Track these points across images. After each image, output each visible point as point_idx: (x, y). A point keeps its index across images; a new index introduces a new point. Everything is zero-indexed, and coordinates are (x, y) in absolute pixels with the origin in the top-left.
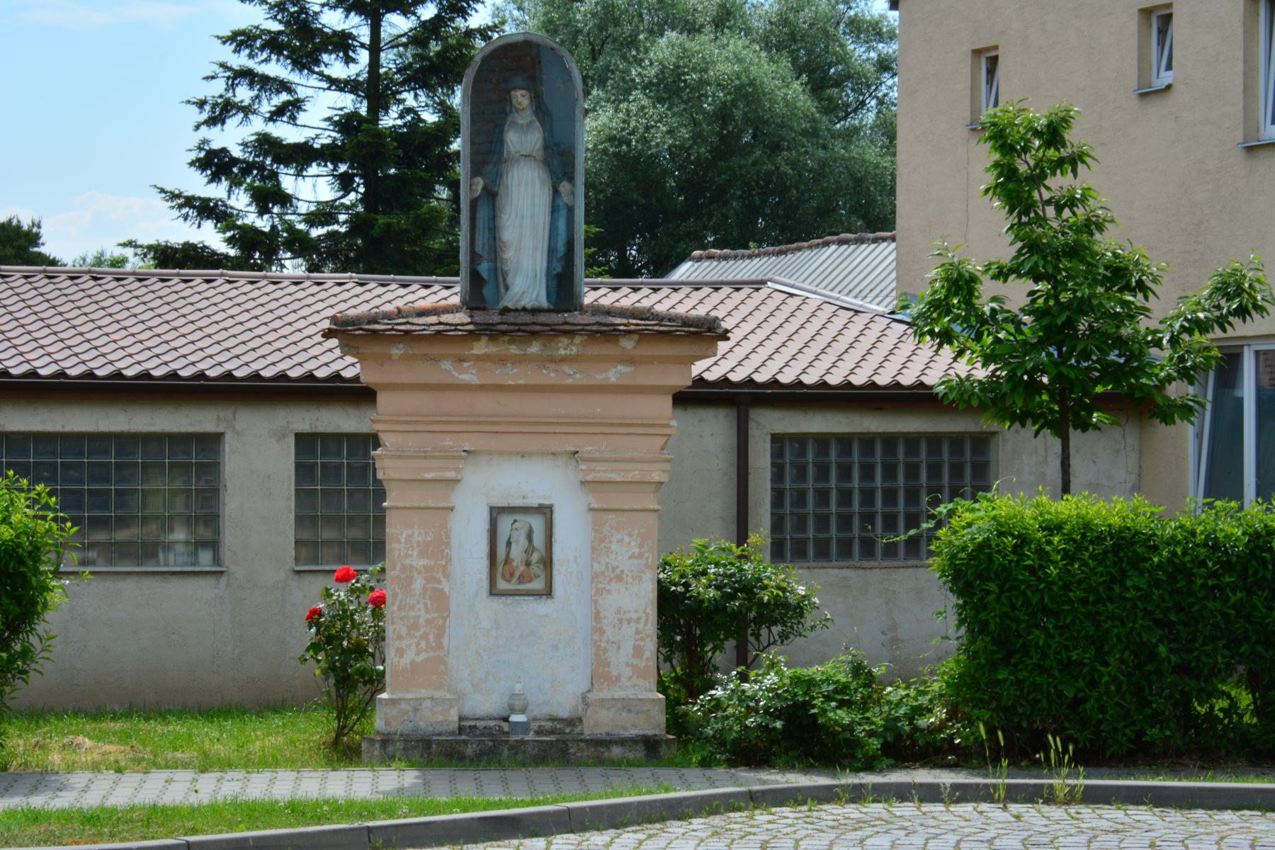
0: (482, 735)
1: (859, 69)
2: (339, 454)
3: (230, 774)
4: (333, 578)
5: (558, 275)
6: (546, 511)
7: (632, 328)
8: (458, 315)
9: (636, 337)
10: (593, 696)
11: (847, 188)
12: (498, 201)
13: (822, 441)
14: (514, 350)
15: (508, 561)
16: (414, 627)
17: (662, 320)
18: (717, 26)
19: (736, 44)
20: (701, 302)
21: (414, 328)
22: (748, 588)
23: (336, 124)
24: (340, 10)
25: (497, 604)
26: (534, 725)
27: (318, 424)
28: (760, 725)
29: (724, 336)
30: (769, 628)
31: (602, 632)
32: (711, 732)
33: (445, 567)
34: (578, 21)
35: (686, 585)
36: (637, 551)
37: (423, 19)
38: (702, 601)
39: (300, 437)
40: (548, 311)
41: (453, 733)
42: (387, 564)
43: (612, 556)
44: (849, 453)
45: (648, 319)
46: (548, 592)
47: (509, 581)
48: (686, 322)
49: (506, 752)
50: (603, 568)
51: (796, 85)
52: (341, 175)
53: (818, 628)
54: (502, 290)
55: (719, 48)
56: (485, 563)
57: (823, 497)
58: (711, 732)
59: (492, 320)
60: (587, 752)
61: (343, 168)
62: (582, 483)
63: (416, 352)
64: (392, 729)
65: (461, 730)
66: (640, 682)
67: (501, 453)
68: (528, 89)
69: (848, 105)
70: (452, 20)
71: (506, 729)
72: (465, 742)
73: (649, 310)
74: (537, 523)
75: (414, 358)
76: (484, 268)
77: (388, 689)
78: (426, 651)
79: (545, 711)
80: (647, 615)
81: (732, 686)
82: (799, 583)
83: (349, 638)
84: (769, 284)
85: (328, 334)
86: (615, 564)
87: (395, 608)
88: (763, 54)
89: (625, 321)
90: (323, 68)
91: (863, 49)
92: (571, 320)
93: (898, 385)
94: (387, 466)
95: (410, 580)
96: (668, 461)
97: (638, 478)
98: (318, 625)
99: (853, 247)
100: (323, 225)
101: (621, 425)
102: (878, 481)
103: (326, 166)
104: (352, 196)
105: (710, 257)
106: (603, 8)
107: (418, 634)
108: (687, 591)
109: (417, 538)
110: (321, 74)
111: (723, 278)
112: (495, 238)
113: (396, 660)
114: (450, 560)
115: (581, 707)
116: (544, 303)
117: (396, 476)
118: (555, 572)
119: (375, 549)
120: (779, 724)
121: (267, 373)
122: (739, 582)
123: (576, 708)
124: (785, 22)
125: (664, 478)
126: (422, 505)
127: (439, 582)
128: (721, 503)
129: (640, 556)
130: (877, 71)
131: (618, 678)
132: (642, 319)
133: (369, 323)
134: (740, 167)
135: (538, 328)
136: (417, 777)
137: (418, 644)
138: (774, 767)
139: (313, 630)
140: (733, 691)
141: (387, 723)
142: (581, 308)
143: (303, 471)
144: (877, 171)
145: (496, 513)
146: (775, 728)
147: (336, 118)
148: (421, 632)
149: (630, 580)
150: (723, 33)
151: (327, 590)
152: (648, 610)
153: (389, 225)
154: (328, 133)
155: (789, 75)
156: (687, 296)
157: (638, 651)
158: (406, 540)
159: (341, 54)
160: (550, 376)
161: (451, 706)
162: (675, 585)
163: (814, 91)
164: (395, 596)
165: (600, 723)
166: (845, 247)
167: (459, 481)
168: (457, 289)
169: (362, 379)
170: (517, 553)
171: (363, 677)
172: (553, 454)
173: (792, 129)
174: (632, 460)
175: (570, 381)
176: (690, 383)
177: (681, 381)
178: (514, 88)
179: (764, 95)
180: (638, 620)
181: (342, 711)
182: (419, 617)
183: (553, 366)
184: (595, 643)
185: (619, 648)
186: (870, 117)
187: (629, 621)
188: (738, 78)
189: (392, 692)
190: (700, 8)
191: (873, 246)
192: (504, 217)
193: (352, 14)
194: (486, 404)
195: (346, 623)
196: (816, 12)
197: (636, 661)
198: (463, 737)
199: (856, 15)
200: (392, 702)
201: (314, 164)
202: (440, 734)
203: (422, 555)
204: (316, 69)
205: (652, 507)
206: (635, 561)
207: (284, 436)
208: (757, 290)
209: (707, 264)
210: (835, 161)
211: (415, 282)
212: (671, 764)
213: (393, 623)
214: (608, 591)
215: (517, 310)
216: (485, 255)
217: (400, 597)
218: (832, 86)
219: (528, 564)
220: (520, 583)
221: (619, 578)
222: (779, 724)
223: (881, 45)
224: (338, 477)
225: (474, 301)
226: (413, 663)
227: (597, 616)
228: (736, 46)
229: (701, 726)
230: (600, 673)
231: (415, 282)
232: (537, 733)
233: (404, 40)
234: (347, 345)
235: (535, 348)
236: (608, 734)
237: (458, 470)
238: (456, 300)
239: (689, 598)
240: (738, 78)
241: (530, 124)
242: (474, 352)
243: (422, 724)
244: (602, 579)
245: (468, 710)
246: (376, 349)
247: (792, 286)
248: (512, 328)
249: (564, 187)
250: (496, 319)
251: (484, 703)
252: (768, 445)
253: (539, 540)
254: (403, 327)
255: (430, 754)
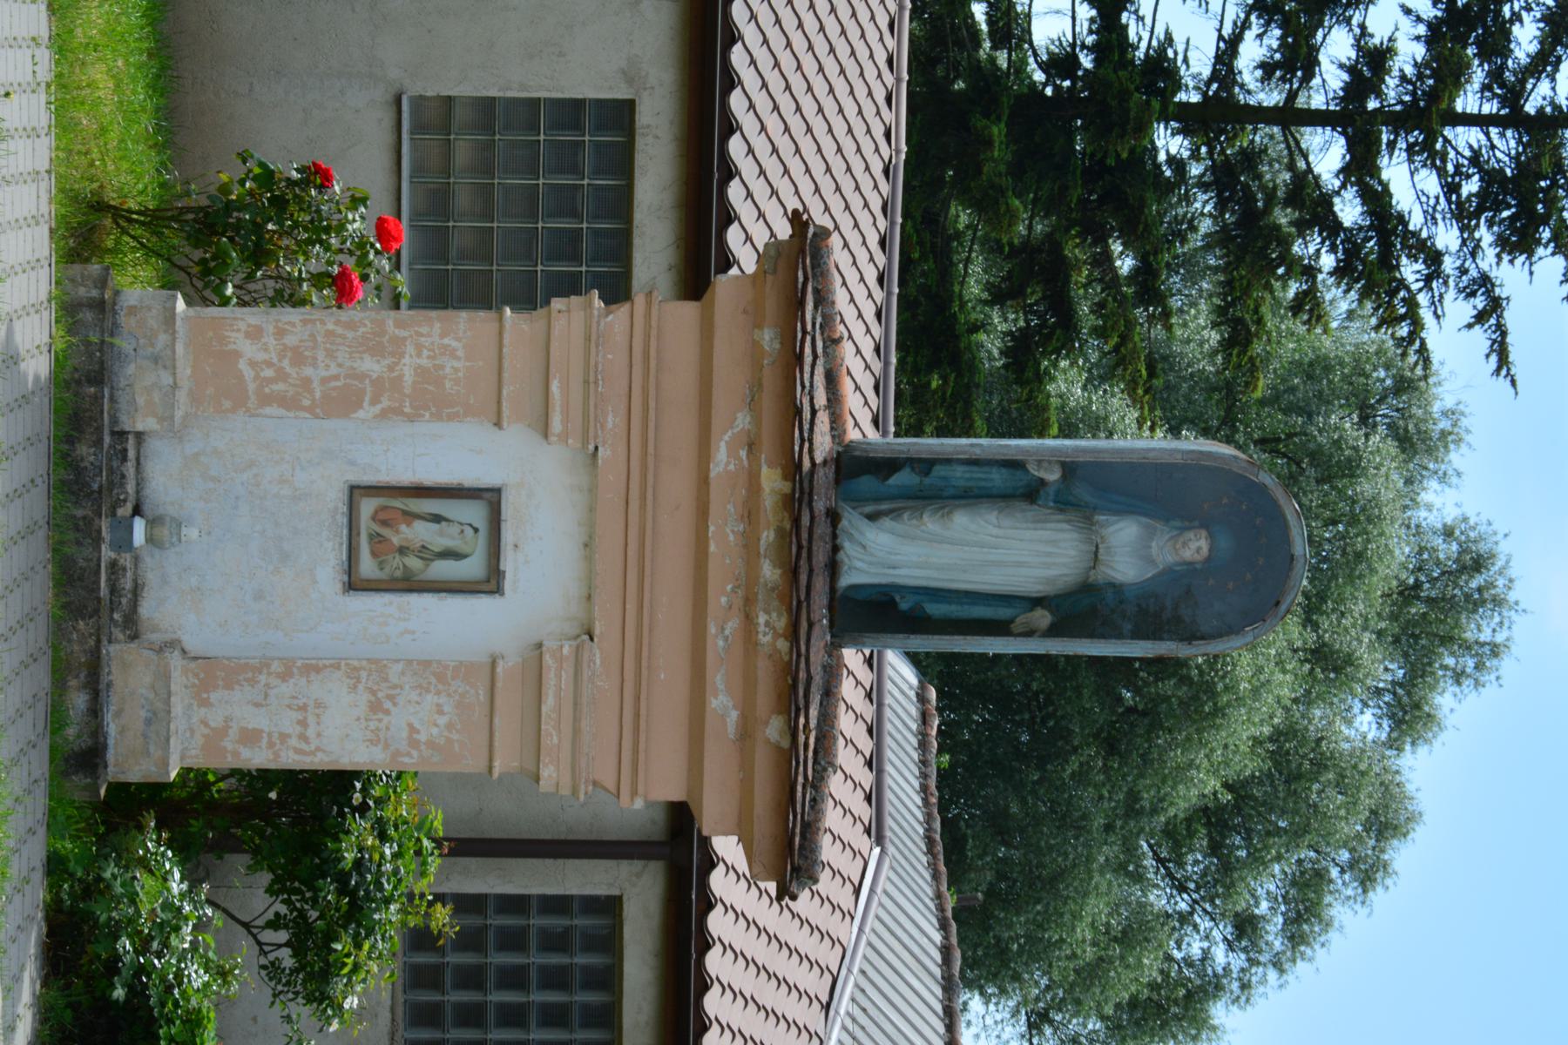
0: (111, 471)
1: (1241, 887)
2: (597, 172)
3: (44, 55)
4: (388, 214)
5: (892, 603)
6: (492, 582)
7: (802, 738)
8: (828, 439)
9: (786, 744)
10: (175, 661)
11: (1041, 865)
12: (1024, 505)
13: (609, 979)
14: (767, 536)
15: (411, 516)
16: (298, 358)
17: (814, 787)
18: (1313, 652)
19: (1285, 686)
20: (857, 388)
21: (807, 369)
22: (356, 913)
23: (1162, 51)
24: (1353, 55)
25: (335, 498)
26: (126, 560)
27: (650, 139)
28: (118, 958)
29: (785, 893)
30: (287, 944)
31: (285, 676)
32: (107, 875)
33: (398, 411)
34: (1327, 416)
35: (363, 809)
36: (423, 737)
37: (1336, 200)
38: (338, 840)
39: (628, 107)
40: (833, 589)
41: (114, 420)
42: (405, 313)
43: (414, 696)
44: (588, 985)
45: (815, 762)
46: (354, 584)
47: (374, 518)
48: (810, 829)
49: (79, 513)
50: (394, 679)
51: (1213, 784)
52: (1076, 57)
53: (287, 1027)
54: (869, 509)
55: (1279, 654)
56: (406, 477)
57: (514, 978)
58: (107, 875)
59: (825, 493)
60: (77, 651)
61: (1086, 61)
62: (540, 646)
63: (767, 372)
64: (123, 319)
65: (120, 435)
66: (199, 740)
67: (592, 509)
68: (1208, 560)
69: (1181, 864)
70: (1333, 249)
71: (120, 512)
72: (98, 443)
73: (832, 764)
74: (474, 567)
75: (757, 366)
76: (903, 478)
77: (192, 312)
78: (257, 377)
79: (151, 577)
80: (312, 753)
81: (187, 908)
82: (370, 984)
83: (282, 234)
84: (877, 850)
85: (798, 220)
86: (401, 700)
87: (331, 327)
88: (1267, 730)
89: (813, 723)
90: (1256, 29)
91: (1272, 888)
92: (816, 631)
93: (704, 987)
94: (572, 316)
95: (377, 351)
96: (575, 791)
97: (545, 741)
98: (305, 183)
99: (938, 972)
100: (990, 22)
101: (637, 715)
102: (538, 997)
103: (1091, 32)
104: (1039, 76)
105: (924, 718)
106: (1349, 460)
107: (286, 363)
108: (354, 810)
109: (450, 365)
110: (1246, 25)
111: (888, 740)
112: (954, 497)
113: (242, 326)
114: (411, 419)
115: (155, 637)
116: (846, 580)
117: (556, 331)
118: (387, 598)
119: (438, 293)
120: (119, 993)
121: (737, 56)
122: (368, 897)
123: (155, 629)
124: (1320, 765)
125: (546, 785)
126: (506, 375)
127: (374, 402)
128: (504, 815)
129: (414, 743)
130: (1237, 915)
131: (205, 703)
132: (816, 752)
133: (816, 291)
134: (1078, 690)
135: (803, 578)
136: (37, 378)
137: (269, 364)
138: (45, 984)
139: (295, 175)
140: (180, 909)
141: (132, 310)
142: (834, 647)
143: (570, 112)
144: (1067, 917)
145: (491, 498)
146: (112, 987)
147: (1170, 53)
148: (288, 369)
149: (373, 725)
150: (1302, 662)
151: (363, 201)
152: (320, 755)
153: (989, 143)
154: (1146, 36)
155: (1230, 774)
156: (867, 367)
157: (250, 737)
158: (446, 347)
159: (1278, 56)
160: (721, 596)
161: (161, 420)
162: (364, 790)
163: (1205, 809)
164: (351, 325)
165: (130, 673)
166: (939, 959)
167: (546, 436)
168: (872, 435)
169: (722, 278)
170: (421, 532)
171: (214, 258)
172: (589, 597)
173: (1142, 776)
174: (576, 731)
175: (712, 629)
176: (705, 833)
177: (712, 813)
178: (1211, 536)
179: (1199, 731)
180: (303, 738)
181: (155, 219)
182: (314, 365)
183: (738, 602)
184: (265, 665)
185: (257, 705)
186: (1158, 899)
187: (303, 723)
188: (1226, 688)
189: (186, 319)
190: (1346, 622)
191: (939, 1008)
192: (993, 517)
193: (1346, 77)
194: (676, 485)
195: (306, 229)
196: (1336, 817)
197: (233, 733)
198: (107, 439)
199: (1331, 881)
200: (170, 317)
201: (1094, 13)
202: (112, 400)
203: (420, 372)
204: (1253, 18)
205: (496, 764)
206: (405, 734)
207: (630, 81)
208: (868, 831)
209: (914, 711)
210: (1087, 845)
211: (890, 259)
212: (56, 796)
213: (305, 322)
214: (355, 687)
215: (834, 536)
216: (927, 481)
217: (350, 335)
218: (1211, 839)
219: (403, 550)
220: (371, 537)
221: (376, 707)
222: (119, 993)
223: (1280, 920)
224: (560, 170)
225: (852, 465)
226: (237, 354)
227: (312, 669)
228: (1280, 685)
229: (119, 856)
230: (214, 672)
231: (890, 259)
232: (113, 565)
233: (1302, 165)
234: (779, 254)
235: (769, 572)
236: (109, 685)
237: (564, 437)
238: (853, 435)
239: (342, 815)
240: (1226, 688)
241: (1151, 561)
242: (765, 470)
243: (131, 369)
244: (373, 677)
245: (153, 445)
246: (772, 304)
247: (872, 890)
248: (805, 535)
249: (1043, 618)
250: (820, 505)
251: (165, 475)
252: (602, 891)
253: (443, 569)
254: (808, 350)
255: (78, 382)
